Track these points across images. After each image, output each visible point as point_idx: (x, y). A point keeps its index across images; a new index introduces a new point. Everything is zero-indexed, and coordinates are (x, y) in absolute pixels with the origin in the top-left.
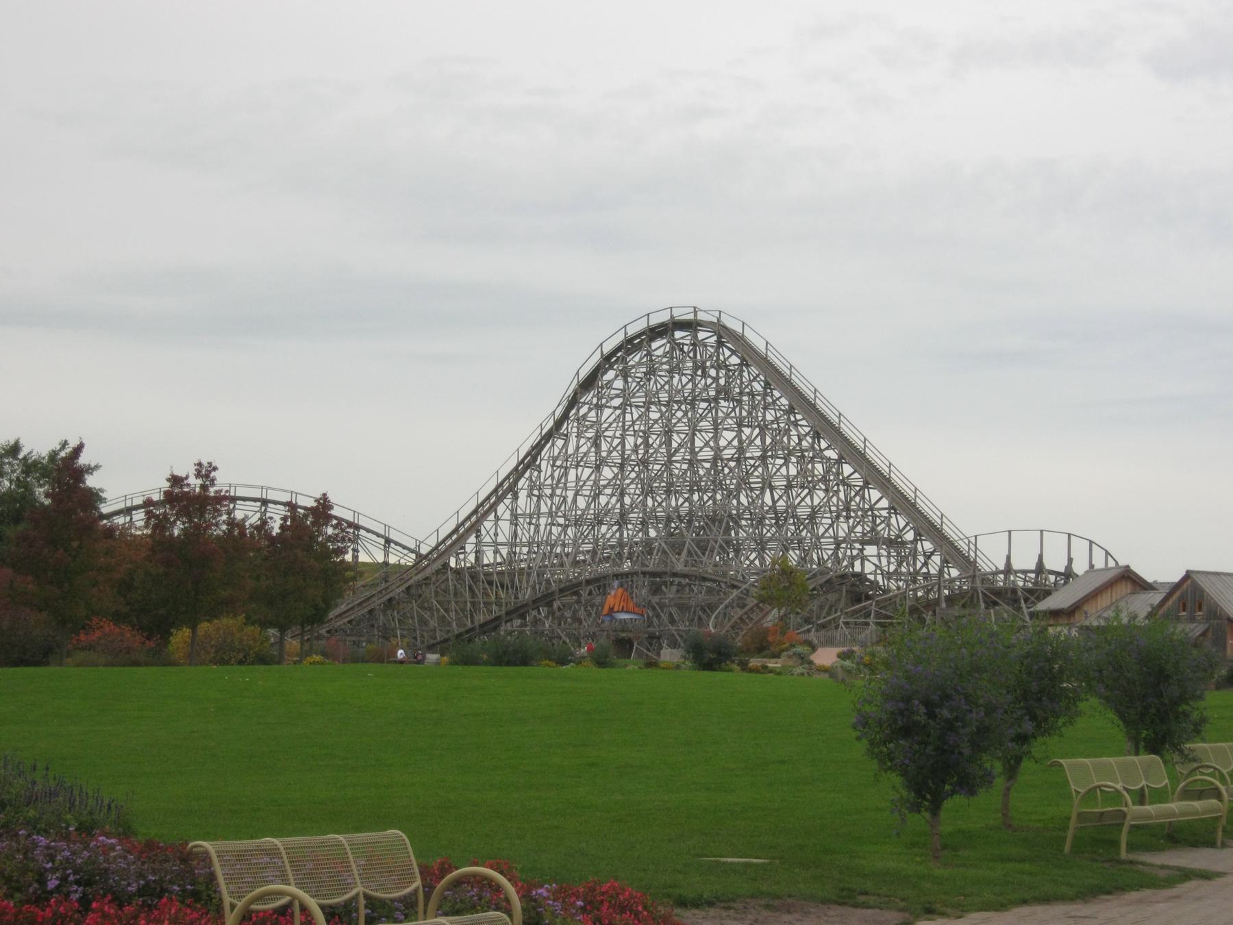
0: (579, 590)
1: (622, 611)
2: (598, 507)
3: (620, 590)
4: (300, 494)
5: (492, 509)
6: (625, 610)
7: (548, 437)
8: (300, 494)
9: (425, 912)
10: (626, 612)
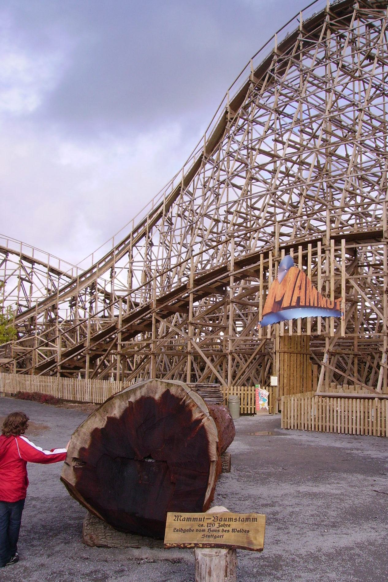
1: (298, 306)
4: (64, 261)
5: (109, 266)
6: (302, 303)
7: (177, 193)
8: (64, 261)
10: (305, 307)
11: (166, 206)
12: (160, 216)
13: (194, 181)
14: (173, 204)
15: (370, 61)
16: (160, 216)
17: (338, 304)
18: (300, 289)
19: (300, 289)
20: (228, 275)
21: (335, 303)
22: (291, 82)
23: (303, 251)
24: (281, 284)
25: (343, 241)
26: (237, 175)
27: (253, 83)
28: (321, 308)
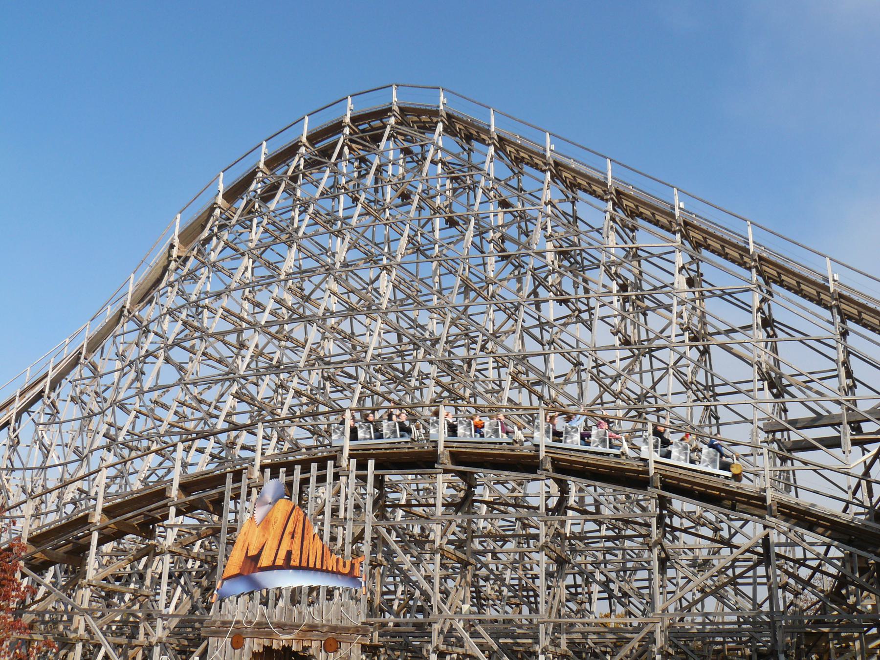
0: (473, 473)
1: (287, 565)
2: (635, 553)
3: (283, 505)
6: (295, 562)
9: (429, 505)
10: (299, 568)
11: (52, 381)
12: (40, 396)
13: (103, 348)
14: (63, 381)
15: (402, 201)
16: (40, 396)
17: (357, 565)
18: (293, 537)
19: (293, 537)
20: (167, 504)
21: (352, 565)
22: (280, 214)
23: (301, 473)
24: (260, 526)
25: (371, 463)
26: (178, 345)
27: (220, 207)
28: (327, 571)
